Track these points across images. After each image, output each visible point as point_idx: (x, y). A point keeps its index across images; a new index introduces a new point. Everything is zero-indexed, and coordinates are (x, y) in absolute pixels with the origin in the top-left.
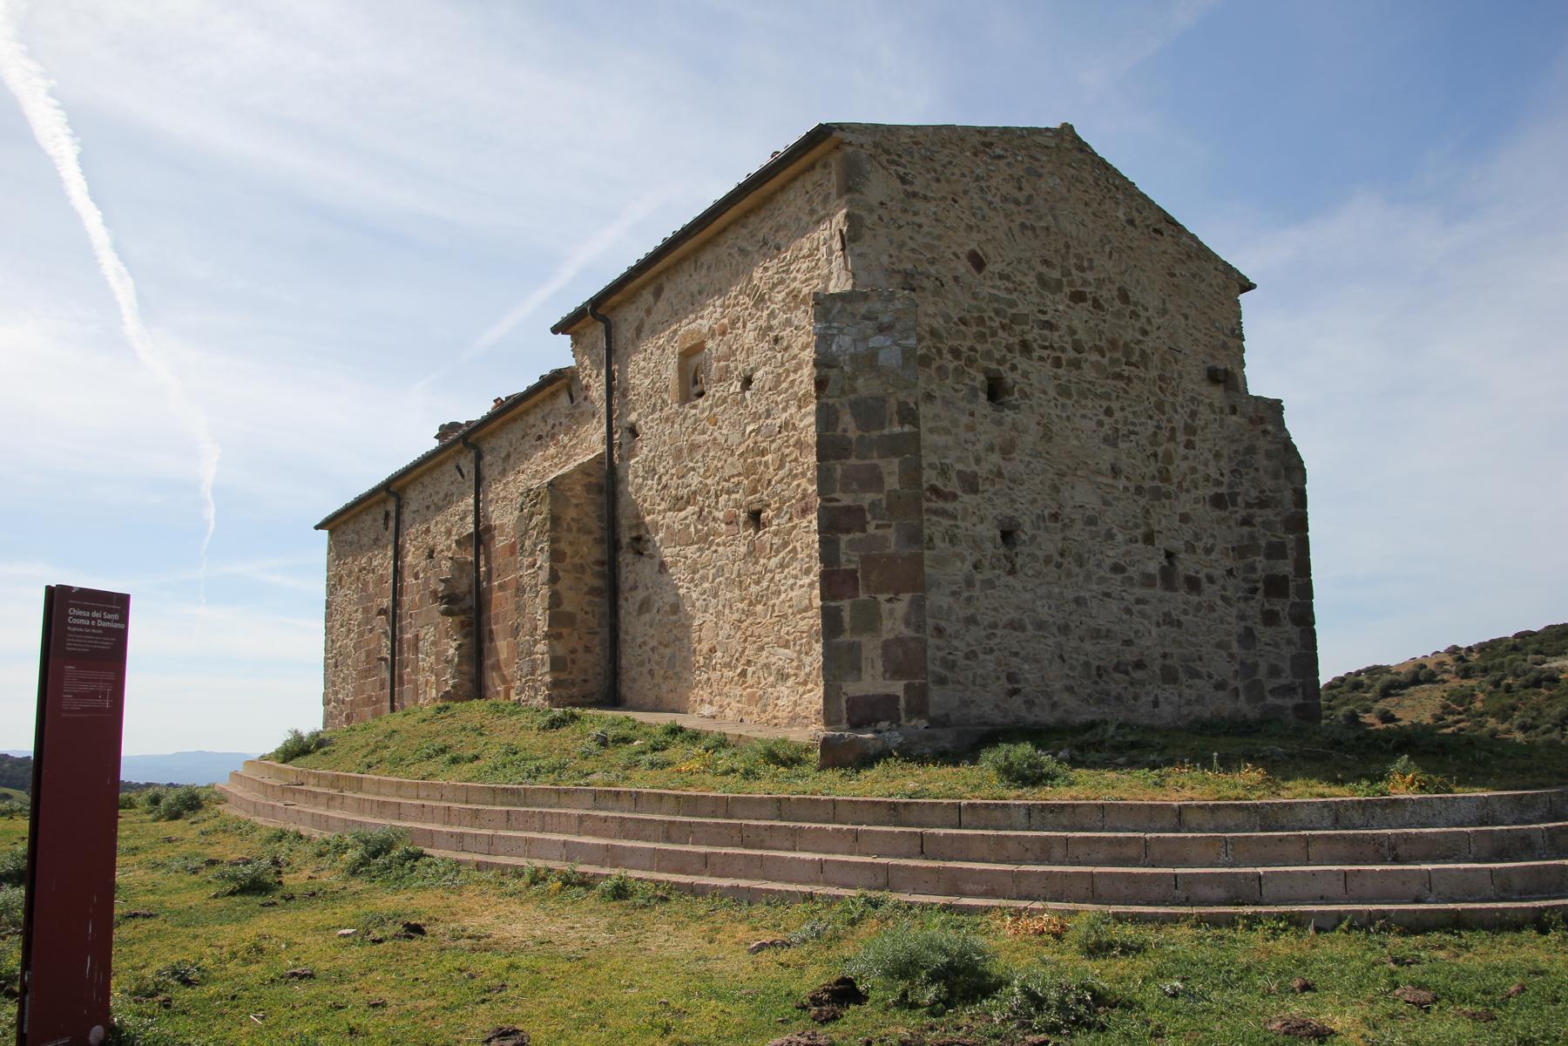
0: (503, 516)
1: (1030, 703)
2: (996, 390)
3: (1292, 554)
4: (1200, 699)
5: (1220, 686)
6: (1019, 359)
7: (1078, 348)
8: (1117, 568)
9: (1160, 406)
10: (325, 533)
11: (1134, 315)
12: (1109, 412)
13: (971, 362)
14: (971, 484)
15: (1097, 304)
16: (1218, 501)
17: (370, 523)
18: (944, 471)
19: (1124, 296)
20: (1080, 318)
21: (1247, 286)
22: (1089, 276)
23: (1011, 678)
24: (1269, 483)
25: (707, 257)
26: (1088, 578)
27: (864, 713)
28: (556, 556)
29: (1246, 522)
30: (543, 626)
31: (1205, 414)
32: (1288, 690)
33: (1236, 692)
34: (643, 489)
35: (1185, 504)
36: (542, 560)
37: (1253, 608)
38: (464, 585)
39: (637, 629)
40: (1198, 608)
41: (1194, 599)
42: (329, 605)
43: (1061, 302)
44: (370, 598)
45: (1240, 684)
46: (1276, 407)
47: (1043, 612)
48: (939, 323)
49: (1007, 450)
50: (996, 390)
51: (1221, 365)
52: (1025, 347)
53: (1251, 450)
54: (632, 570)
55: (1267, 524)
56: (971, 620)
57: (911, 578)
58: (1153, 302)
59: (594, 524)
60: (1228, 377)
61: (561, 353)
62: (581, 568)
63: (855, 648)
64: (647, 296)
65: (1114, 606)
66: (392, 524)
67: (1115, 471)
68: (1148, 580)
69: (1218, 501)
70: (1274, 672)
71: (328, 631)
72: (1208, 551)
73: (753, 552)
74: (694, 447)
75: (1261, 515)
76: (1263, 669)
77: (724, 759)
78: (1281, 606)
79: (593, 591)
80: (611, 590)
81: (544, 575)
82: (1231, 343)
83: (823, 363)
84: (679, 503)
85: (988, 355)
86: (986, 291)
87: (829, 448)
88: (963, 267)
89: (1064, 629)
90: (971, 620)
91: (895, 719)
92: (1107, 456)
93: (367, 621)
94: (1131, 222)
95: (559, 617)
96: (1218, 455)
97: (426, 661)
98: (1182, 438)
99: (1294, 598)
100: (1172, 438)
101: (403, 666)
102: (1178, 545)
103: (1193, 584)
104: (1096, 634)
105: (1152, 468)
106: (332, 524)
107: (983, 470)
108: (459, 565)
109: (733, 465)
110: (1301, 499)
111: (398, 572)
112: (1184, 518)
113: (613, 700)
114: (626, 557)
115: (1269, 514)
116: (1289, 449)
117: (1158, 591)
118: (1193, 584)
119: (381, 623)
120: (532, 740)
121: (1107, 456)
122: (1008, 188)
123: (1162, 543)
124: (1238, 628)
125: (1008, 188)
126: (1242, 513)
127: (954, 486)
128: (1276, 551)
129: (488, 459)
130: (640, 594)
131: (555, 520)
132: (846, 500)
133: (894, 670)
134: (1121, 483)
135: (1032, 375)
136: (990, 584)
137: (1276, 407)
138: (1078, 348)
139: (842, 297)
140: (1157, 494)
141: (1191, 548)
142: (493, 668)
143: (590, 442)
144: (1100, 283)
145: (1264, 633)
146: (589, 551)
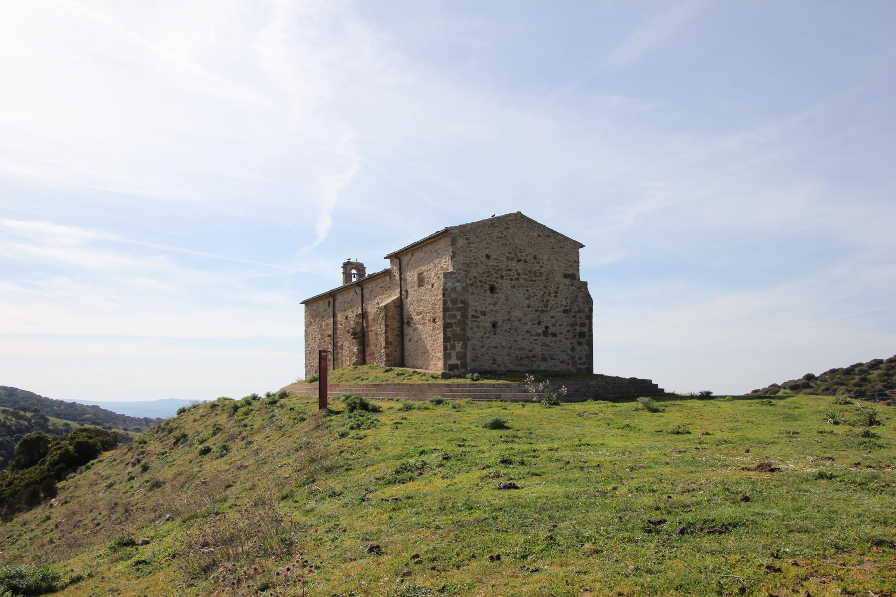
0: (372, 309)
1: (499, 366)
2: (492, 289)
3: (587, 326)
4: (555, 366)
5: (563, 362)
6: (500, 281)
7: (518, 274)
8: (527, 332)
9: (546, 287)
10: (303, 305)
11: (538, 262)
12: (527, 291)
13: (485, 283)
14: (484, 314)
15: (525, 262)
16: (565, 311)
17: (322, 305)
18: (476, 311)
19: (535, 257)
20: (519, 267)
21: (582, 246)
22: (524, 254)
23: (494, 360)
24: (582, 306)
25: (424, 249)
26: (518, 335)
27: (452, 367)
28: (387, 326)
29: (574, 317)
30: (383, 345)
31: (562, 287)
32: (584, 363)
33: (568, 364)
34: (411, 307)
35: (553, 313)
36: (383, 327)
37: (575, 341)
38: (358, 329)
39: (408, 346)
40: (555, 341)
41: (554, 339)
42: (306, 332)
43: (514, 263)
44: (324, 330)
45: (570, 362)
46: (585, 284)
47: (504, 344)
48: (476, 275)
49: (495, 304)
50: (492, 289)
51: (570, 271)
52: (502, 277)
53: (577, 296)
54: (408, 331)
55: (580, 317)
56: (483, 346)
57: (465, 339)
58: (545, 257)
59: (397, 317)
60: (573, 276)
61: (387, 264)
62: (393, 329)
63: (450, 354)
64: (410, 255)
65: (526, 342)
66: (331, 305)
67: (529, 306)
68: (538, 334)
69: (565, 311)
70: (580, 358)
71: (306, 341)
72: (560, 326)
73: (434, 328)
74: (421, 300)
75: (578, 315)
76: (577, 358)
77: (424, 377)
78: (583, 340)
79: (397, 335)
80: (402, 335)
81: (383, 331)
82: (575, 265)
83: (444, 290)
84: (418, 314)
85: (490, 281)
86: (491, 264)
87: (445, 309)
88: (484, 259)
89: (510, 348)
90: (483, 346)
91: (458, 368)
92: (527, 302)
93: (323, 338)
94: (539, 236)
95: (388, 343)
96: (566, 298)
97: (345, 352)
98: (553, 295)
99: (587, 338)
100: (549, 295)
101: (338, 354)
102: (549, 324)
103: (554, 335)
104: (520, 349)
105: (542, 304)
106: (307, 303)
107: (487, 310)
108: (357, 323)
109: (430, 306)
110: (591, 310)
111: (335, 323)
112: (552, 317)
113: (402, 364)
114: (405, 326)
115: (581, 314)
116: (589, 296)
117: (542, 337)
118: (554, 335)
119: (328, 340)
120: (381, 375)
121: (527, 302)
122: (499, 235)
123: (543, 325)
124: (570, 346)
125: (499, 235)
126: (573, 314)
127: (479, 314)
128: (583, 325)
129: (365, 290)
130: (409, 337)
131: (386, 316)
132: (449, 321)
133: (458, 359)
134: (530, 309)
135: (505, 285)
136: (488, 338)
137: (585, 284)
138: (518, 274)
139: (450, 273)
140: (543, 311)
141: (554, 325)
142: (369, 355)
143: (395, 296)
144: (527, 256)
145: (578, 348)
146: (396, 324)
